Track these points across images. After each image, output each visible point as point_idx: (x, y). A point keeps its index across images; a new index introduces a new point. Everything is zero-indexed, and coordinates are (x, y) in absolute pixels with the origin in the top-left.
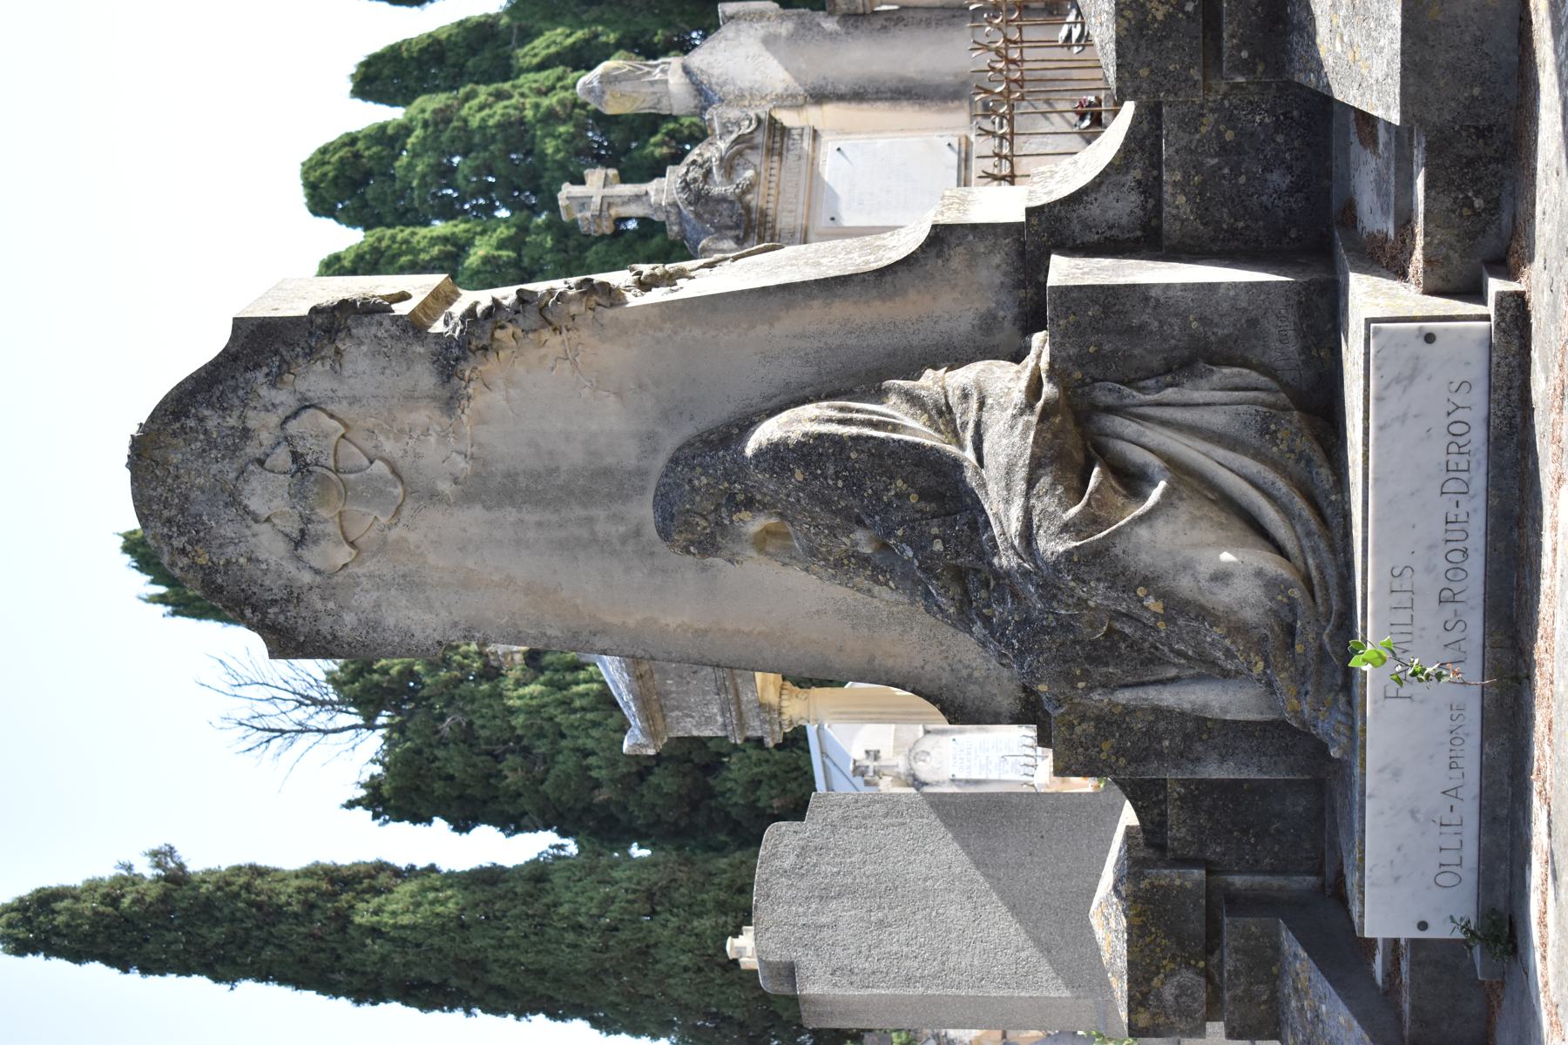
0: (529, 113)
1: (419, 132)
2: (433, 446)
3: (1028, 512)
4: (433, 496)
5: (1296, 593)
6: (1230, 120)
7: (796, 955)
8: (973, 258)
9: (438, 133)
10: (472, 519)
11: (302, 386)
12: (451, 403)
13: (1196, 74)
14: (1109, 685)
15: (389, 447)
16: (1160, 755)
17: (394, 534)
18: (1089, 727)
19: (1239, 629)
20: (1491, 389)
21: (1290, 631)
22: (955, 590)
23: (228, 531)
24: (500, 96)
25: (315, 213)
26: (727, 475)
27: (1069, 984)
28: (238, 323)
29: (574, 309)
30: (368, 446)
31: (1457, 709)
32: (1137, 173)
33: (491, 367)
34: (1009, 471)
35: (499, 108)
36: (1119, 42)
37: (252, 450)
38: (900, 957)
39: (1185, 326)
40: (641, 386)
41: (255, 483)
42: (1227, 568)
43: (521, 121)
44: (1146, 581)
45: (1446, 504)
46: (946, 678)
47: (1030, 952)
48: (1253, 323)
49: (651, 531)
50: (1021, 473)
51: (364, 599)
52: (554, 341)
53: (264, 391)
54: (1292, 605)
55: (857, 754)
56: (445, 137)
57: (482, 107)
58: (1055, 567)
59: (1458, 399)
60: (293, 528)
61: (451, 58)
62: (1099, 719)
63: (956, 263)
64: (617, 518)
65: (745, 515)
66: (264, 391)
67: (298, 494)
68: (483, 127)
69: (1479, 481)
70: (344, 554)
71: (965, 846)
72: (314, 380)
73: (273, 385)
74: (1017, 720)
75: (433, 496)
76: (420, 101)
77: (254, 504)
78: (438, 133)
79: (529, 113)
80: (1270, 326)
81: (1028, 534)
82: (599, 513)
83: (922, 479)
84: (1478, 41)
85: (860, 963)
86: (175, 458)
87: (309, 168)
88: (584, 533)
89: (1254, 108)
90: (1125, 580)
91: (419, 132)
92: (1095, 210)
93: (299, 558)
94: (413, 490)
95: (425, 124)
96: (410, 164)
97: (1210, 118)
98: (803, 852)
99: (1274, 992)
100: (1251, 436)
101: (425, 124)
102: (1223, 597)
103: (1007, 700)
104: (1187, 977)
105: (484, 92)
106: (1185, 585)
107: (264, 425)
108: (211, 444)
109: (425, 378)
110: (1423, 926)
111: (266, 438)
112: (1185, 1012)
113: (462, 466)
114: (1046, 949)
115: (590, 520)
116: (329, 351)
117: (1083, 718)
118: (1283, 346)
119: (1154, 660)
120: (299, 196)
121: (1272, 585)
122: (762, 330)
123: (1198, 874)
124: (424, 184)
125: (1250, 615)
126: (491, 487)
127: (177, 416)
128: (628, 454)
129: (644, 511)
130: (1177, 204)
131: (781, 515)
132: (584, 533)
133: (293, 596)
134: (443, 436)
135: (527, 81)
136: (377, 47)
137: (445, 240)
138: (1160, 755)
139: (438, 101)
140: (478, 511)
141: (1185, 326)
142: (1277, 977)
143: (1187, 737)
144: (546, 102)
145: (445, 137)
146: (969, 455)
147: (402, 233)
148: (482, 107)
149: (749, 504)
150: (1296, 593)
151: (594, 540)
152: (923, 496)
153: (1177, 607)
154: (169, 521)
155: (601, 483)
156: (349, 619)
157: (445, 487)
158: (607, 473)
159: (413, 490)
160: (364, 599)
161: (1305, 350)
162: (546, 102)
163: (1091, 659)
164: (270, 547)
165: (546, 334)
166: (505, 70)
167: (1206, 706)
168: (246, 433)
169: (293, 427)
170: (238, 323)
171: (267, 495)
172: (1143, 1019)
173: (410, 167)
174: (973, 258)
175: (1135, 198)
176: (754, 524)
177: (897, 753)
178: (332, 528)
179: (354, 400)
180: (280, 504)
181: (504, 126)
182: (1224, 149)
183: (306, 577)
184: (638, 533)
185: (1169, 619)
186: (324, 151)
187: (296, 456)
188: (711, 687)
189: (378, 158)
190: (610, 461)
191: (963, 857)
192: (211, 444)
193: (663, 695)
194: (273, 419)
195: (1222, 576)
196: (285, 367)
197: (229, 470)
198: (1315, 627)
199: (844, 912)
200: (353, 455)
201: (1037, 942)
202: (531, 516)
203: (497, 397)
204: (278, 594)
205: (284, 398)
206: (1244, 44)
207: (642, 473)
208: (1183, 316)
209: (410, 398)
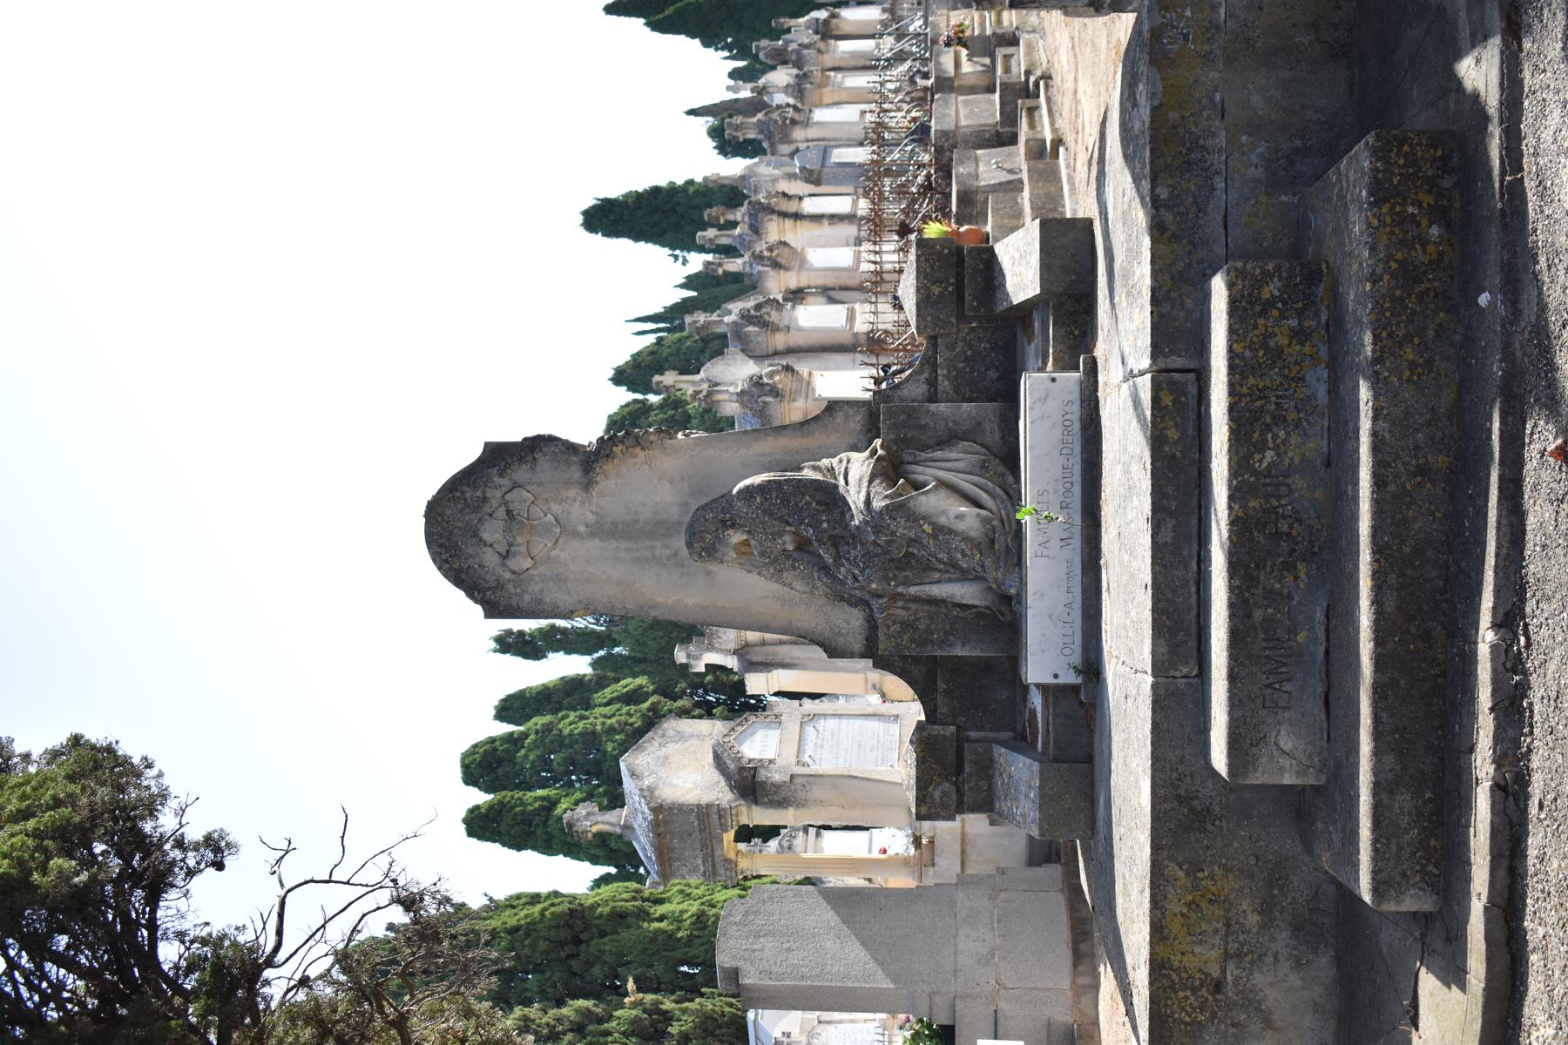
0: (599, 728)
1: (532, 737)
2: (578, 509)
3: (868, 494)
4: (575, 534)
5: (995, 522)
6: (970, 346)
7: (739, 964)
8: (847, 418)
9: (544, 737)
10: (594, 545)
11: (515, 476)
12: (587, 486)
13: (953, 320)
14: (906, 583)
15: (555, 508)
16: (932, 642)
17: (553, 554)
18: (897, 627)
19: (966, 539)
20: (1082, 401)
21: (992, 541)
22: (832, 550)
23: (470, 551)
24: (582, 718)
25: (467, 783)
26: (723, 511)
27: (893, 981)
28: (487, 444)
29: (652, 438)
30: (545, 508)
31: (1070, 562)
32: (926, 375)
33: (609, 467)
34: (860, 480)
35: (581, 724)
36: (918, 304)
37: (487, 509)
38: (798, 966)
39: (946, 425)
40: (682, 478)
41: (487, 525)
42: (962, 517)
43: (594, 733)
44: (924, 518)
45: (1063, 459)
46: (827, 633)
47: (872, 965)
48: (979, 424)
49: (684, 552)
50: (866, 479)
51: (535, 588)
52: (642, 454)
53: (496, 479)
54: (993, 530)
55: (777, 1034)
56: (547, 740)
57: (571, 723)
58: (881, 513)
59: (1067, 409)
60: (503, 549)
61: (555, 698)
62: (902, 623)
63: (838, 420)
64: (665, 546)
65: (731, 532)
66: (496, 479)
67: (508, 530)
68: (571, 735)
69: (1078, 449)
70: (527, 563)
71: (837, 912)
72: (521, 473)
73: (501, 476)
74: (862, 656)
75: (575, 534)
76: (534, 720)
77: (486, 536)
78: (544, 737)
79: (599, 728)
80: (987, 425)
81: (868, 502)
82: (658, 544)
83: (819, 496)
84: (1074, 255)
85: (775, 969)
86: (448, 512)
87: (465, 756)
88: (649, 554)
89: (981, 340)
90: (914, 518)
91: (532, 737)
92: (906, 392)
93: (504, 565)
94: (566, 530)
95: (537, 732)
96: (527, 756)
97: (960, 344)
98: (747, 913)
99: (990, 785)
100: (977, 470)
101: (537, 732)
102: (961, 526)
103: (858, 644)
104: (946, 786)
105: (572, 715)
106: (943, 520)
107: (494, 496)
108: (468, 505)
109: (576, 473)
110: (1056, 676)
111: (494, 503)
112: (945, 806)
113: (591, 518)
114: (881, 963)
115: (652, 547)
116: (530, 458)
117: (894, 622)
118: (993, 436)
119: (929, 568)
120: (457, 772)
121: (984, 521)
122: (743, 451)
123: (952, 728)
124: (533, 766)
125: (973, 534)
126: (604, 529)
127: (451, 491)
128: (674, 514)
129: (680, 542)
130: (944, 385)
131: (749, 532)
132: (649, 554)
133: (500, 585)
134: (583, 503)
135: (598, 711)
136: (512, 690)
137: (543, 798)
138: (932, 642)
139: (547, 719)
140: (597, 541)
141: (946, 425)
142: (992, 776)
143: (945, 633)
144: (609, 722)
145: (547, 740)
146: (842, 482)
147: (518, 794)
148: (571, 723)
149: (733, 526)
150: (995, 522)
151: (654, 557)
152: (818, 503)
153: (939, 530)
154: (441, 545)
155: (659, 528)
156: (527, 598)
157: (581, 529)
158: (662, 523)
159: (566, 530)
160: (535, 588)
161: (1003, 437)
162: (609, 722)
163: (898, 568)
164: (490, 559)
165: (638, 450)
166: (588, 705)
167: (953, 595)
168: (485, 500)
169: (508, 497)
170: (487, 444)
171: (492, 532)
172: (924, 810)
173: (526, 757)
174: (847, 418)
175: (925, 387)
176: (736, 537)
177: (801, 1033)
178: (523, 549)
179: (540, 484)
180: (498, 536)
181: (583, 734)
182: (967, 359)
183: (507, 575)
184: (676, 554)
185: (934, 536)
186: (475, 746)
187: (509, 512)
188: (698, 846)
189: (507, 751)
190: (665, 516)
191: (836, 917)
192: (468, 505)
193: (671, 850)
194: (499, 494)
195: (960, 517)
196: (508, 466)
197: (474, 518)
198: (1006, 544)
199: (768, 944)
200: (537, 511)
201: (876, 960)
202: (623, 545)
203: (611, 483)
204: (492, 584)
205: (505, 482)
206: (975, 299)
207: (680, 523)
208: (945, 420)
209: (568, 483)
